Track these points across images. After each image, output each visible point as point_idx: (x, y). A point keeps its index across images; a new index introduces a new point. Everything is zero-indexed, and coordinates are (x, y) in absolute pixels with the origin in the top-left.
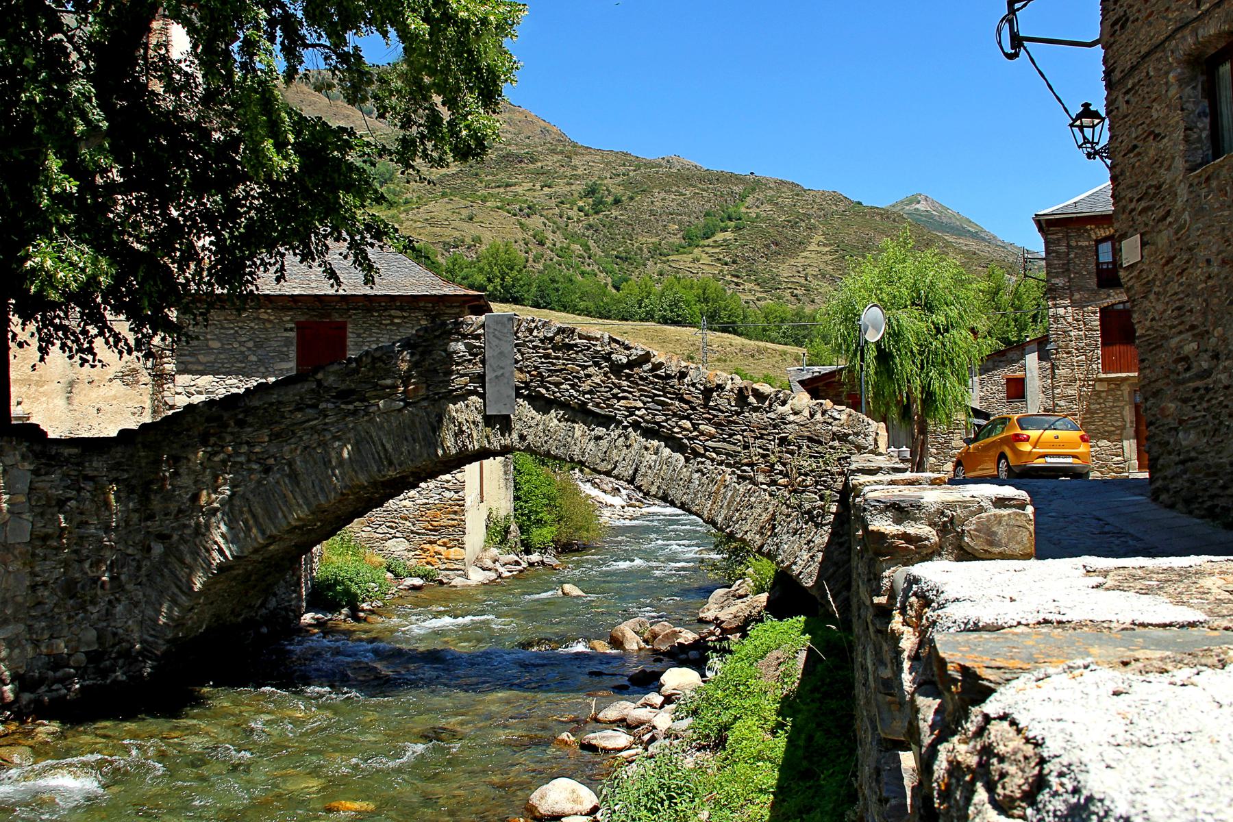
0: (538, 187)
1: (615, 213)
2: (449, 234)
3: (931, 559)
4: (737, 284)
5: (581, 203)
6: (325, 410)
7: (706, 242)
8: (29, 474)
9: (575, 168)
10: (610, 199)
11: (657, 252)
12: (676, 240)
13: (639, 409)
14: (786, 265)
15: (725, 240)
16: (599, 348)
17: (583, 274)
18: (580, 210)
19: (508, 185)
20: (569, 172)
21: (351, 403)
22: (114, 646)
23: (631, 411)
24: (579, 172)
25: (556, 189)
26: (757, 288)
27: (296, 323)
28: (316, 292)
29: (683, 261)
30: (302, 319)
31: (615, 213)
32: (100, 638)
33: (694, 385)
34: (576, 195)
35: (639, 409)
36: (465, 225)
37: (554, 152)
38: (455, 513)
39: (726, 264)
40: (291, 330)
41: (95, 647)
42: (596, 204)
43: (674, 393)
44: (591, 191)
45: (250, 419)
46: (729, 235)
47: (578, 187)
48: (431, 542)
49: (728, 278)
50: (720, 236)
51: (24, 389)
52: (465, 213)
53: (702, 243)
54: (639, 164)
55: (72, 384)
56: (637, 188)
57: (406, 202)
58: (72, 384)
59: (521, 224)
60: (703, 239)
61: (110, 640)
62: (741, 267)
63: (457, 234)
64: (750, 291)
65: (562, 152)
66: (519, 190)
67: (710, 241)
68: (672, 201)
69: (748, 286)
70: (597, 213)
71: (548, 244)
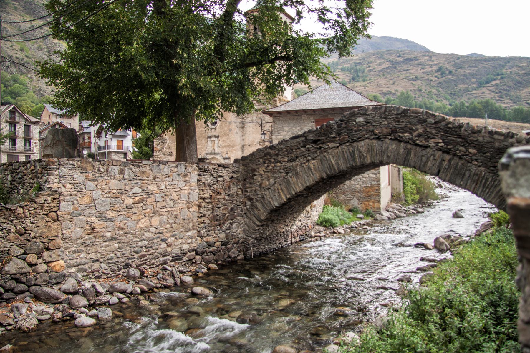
0: (419, 70)
1: (450, 77)
2: (385, 90)
3: (499, 57)
4: (501, 101)
5: (436, 74)
6: (308, 148)
7: (488, 85)
8: (197, 176)
9: (433, 61)
10: (447, 72)
11: (467, 90)
12: (475, 86)
13: (440, 143)
14: (524, 91)
15: (496, 84)
16: (421, 117)
17: (437, 101)
18: (436, 77)
19: (407, 70)
20: (431, 63)
21: (318, 145)
22: (232, 239)
23: (437, 144)
24: (435, 63)
25: (426, 70)
26: (510, 101)
27: (316, 120)
28: (322, 108)
29: (478, 92)
30: (317, 118)
31: (450, 77)
32: (227, 236)
33: (466, 131)
34: (434, 71)
35: (440, 143)
36: (392, 86)
37: (425, 56)
38: (377, 190)
39: (496, 93)
40: (313, 122)
41: (225, 239)
42: (442, 74)
43: (458, 135)
44: (440, 69)
45: (280, 153)
46: (498, 82)
47: (435, 68)
48: (367, 201)
49: (498, 98)
50: (494, 83)
51: (228, 149)
52: (392, 82)
53: (486, 85)
54: (459, 57)
55: (243, 146)
56: (458, 66)
57: (370, 79)
58: (243, 146)
59: (413, 84)
60: (486, 84)
61: (230, 237)
62: (504, 93)
63: (389, 89)
64: (507, 103)
65: (428, 56)
66: (412, 71)
67: (490, 85)
68: (473, 70)
69: (506, 101)
70: (442, 77)
71: (423, 91)
